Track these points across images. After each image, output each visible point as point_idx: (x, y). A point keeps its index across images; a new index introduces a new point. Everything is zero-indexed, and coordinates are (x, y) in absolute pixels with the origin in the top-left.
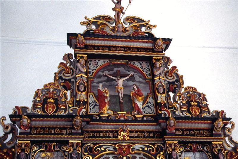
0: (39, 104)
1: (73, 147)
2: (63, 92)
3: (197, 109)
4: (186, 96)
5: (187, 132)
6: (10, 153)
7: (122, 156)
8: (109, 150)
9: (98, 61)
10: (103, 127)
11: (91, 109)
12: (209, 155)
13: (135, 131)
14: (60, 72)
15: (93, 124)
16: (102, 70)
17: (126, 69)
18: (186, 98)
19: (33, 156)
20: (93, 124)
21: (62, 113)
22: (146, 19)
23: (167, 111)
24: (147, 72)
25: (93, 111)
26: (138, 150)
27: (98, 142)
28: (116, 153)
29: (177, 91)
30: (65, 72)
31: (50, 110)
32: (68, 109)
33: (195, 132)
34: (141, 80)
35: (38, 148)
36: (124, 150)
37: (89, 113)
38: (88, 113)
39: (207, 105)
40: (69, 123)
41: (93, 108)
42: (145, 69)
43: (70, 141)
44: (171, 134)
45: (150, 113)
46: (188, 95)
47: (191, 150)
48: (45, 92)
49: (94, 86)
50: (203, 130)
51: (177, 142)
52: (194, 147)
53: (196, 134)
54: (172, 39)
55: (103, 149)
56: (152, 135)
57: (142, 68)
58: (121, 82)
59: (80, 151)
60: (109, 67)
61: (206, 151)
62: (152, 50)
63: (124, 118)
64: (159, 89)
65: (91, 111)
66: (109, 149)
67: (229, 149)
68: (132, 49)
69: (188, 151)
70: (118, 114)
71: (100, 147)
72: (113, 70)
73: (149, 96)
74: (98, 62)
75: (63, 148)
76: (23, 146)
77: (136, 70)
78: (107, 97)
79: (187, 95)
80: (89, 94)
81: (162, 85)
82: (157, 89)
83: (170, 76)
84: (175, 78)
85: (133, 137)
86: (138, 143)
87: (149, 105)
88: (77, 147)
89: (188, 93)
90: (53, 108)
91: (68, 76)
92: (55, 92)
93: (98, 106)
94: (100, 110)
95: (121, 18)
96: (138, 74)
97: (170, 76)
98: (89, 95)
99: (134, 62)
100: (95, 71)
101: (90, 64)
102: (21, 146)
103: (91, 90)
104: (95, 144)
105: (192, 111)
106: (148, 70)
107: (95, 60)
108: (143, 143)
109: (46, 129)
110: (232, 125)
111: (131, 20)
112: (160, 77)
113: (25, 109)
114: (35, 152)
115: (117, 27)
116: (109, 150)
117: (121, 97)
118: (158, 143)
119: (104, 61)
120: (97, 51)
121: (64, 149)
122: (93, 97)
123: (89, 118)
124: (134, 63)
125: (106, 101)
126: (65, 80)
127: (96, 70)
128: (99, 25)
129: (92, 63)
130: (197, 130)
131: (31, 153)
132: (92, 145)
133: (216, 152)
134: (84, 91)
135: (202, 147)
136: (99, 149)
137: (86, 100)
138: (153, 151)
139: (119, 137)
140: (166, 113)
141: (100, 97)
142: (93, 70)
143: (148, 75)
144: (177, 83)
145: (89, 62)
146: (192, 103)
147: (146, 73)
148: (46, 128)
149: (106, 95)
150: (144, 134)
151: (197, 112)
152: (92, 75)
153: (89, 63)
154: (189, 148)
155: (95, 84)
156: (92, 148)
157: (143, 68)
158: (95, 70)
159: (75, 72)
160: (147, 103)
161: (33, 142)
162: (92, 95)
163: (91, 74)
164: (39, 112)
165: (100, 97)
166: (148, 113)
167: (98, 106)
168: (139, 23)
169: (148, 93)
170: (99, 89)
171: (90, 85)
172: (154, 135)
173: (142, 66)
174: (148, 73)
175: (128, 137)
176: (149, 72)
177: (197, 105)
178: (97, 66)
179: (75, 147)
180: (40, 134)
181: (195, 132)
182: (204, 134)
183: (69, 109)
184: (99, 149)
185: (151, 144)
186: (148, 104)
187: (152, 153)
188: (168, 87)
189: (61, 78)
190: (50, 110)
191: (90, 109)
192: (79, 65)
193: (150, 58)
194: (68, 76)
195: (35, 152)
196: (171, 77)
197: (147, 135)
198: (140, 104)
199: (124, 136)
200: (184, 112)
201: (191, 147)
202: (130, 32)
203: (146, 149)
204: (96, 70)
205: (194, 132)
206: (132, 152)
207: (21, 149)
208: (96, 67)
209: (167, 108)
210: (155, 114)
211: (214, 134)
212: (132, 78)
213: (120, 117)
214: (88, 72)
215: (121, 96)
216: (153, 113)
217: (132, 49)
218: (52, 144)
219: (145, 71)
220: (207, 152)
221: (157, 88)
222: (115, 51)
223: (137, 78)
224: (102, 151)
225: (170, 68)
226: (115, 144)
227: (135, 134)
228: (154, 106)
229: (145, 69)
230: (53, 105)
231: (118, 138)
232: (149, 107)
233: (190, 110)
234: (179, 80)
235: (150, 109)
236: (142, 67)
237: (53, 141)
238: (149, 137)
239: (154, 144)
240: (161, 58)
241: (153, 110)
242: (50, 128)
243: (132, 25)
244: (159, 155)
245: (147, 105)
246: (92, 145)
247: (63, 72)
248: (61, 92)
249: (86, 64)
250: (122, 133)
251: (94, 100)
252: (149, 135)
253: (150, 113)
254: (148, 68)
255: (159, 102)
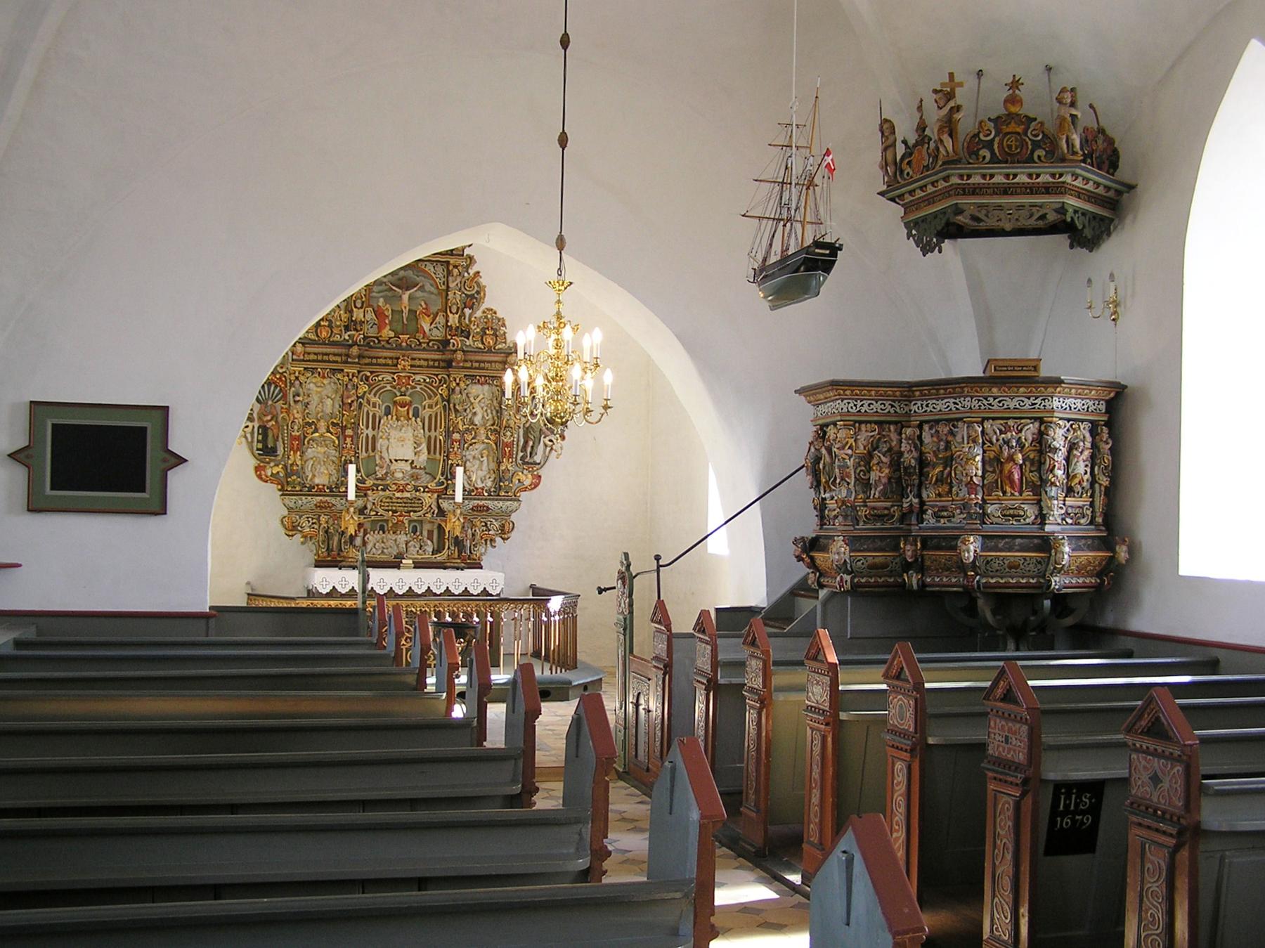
1: (348, 376)
3: (492, 339)
5: (477, 365)
23: (456, 341)
34: (433, 289)
39: (505, 333)
55: (380, 379)
56: (436, 364)
78: (387, 317)
82: (450, 307)
84: (476, 288)
87: (438, 326)
88: (353, 376)
104: (372, 373)
117: (406, 311)
123: (368, 343)
125: (387, 321)
132: (369, 374)
141: (379, 313)
146: (488, 332)
148: (319, 353)
149: (387, 314)
155: (374, 294)
156: (369, 377)
165: (379, 313)
174: (442, 282)
190: (324, 334)
193: (448, 263)
197: (431, 363)
198: (426, 327)
199: (404, 366)
203: (428, 380)
220: (497, 386)
224: (379, 381)
226: (394, 373)
239: (437, 375)
246: (369, 374)
255: (449, 324)
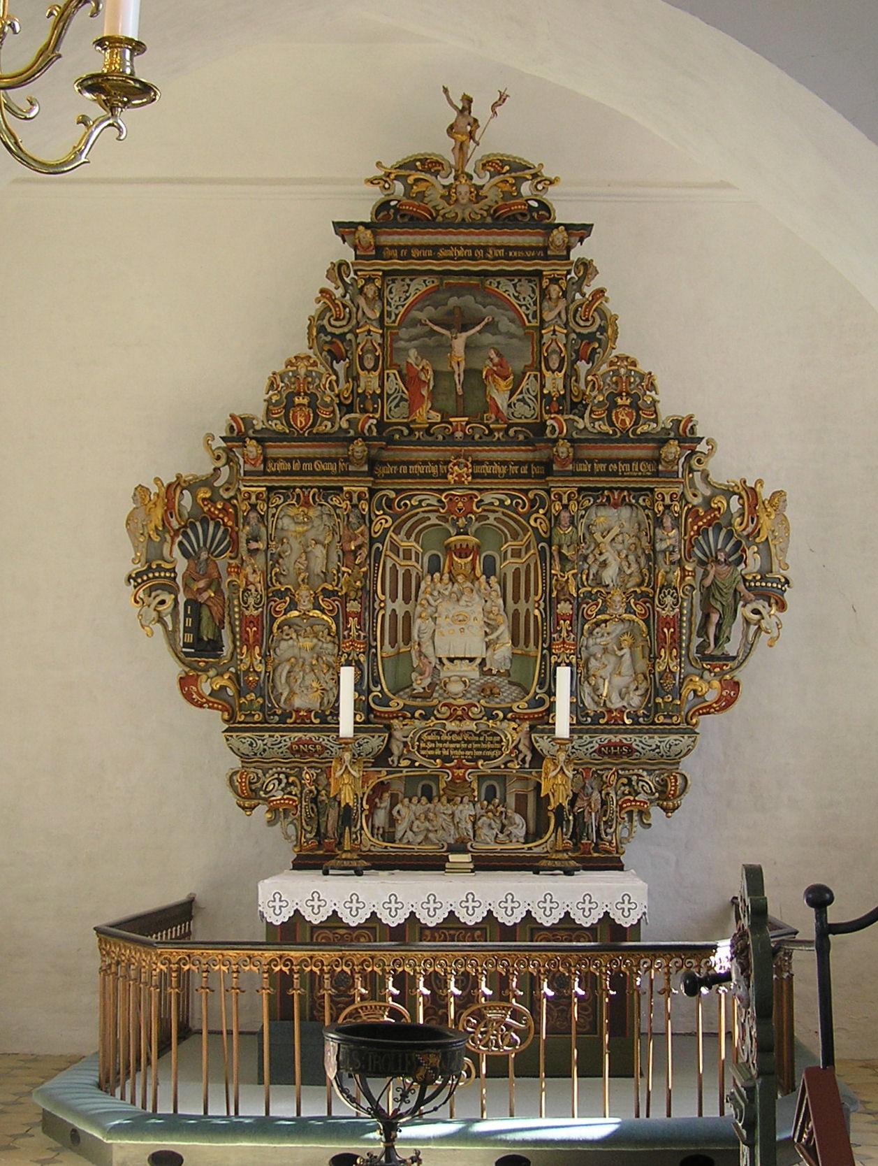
0: (245, 786)
2: (327, 378)
4: (608, 380)
5: (602, 467)
6: (231, 510)
7: (455, 518)
8: (428, 505)
9: (409, 282)
10: (415, 454)
11: (393, 408)
12: (647, 516)
13: (488, 461)
14: (321, 316)
15: (392, 450)
16: (418, 306)
17: (479, 299)
18: (609, 385)
19: (273, 516)
20: (392, 450)
21: (326, 427)
22: (533, 160)
24: (528, 309)
25: (396, 414)
26: (492, 504)
27: (404, 487)
28: (441, 510)
29: (598, 358)
30: (332, 316)
31: (301, 423)
32: (338, 420)
33: (620, 465)
34: (513, 328)
35: (282, 500)
36: (460, 504)
37: (388, 418)
38: (385, 420)
39: (654, 402)
40: (341, 450)
41: (395, 407)
42: (524, 299)
43: (345, 488)
44: (564, 473)
45: (526, 418)
46: (614, 379)
47: (610, 503)
48: (290, 378)
49: (399, 349)
50: (639, 460)
51: (574, 490)
52: (614, 499)
53: (622, 472)
54: (592, 225)
55: (415, 503)
56: (524, 471)
57: (517, 298)
58: (459, 343)
59: (367, 510)
60: (440, 296)
61: (642, 506)
62: (542, 252)
63: (465, 433)
64: (550, 360)
65: (392, 413)
66: (428, 502)
67: (696, 501)
68: (491, 252)
69: (603, 505)
70: (450, 423)
71: (410, 498)
72: (446, 304)
73: (528, 374)
74: (409, 285)
75: (332, 500)
76: (253, 498)
77: (504, 303)
79: (612, 377)
80: (386, 372)
81: (557, 349)
82: (546, 359)
83: (584, 318)
84: (598, 321)
85: (481, 476)
86: (492, 489)
87: (526, 396)
88: (359, 501)
89: (616, 373)
90: (307, 420)
91: (341, 327)
92: (310, 379)
93: (406, 400)
94: (410, 413)
95: (469, 156)
96: (506, 313)
97: (584, 318)
98: (388, 374)
99: (498, 279)
100: (402, 310)
101: (391, 292)
102: (249, 498)
103: (391, 360)
104: (398, 492)
105: (617, 418)
106: (531, 302)
107: (403, 280)
108: (503, 489)
109: (296, 462)
110: (710, 447)
111: (495, 165)
112: (557, 328)
113: (247, 421)
114: (277, 507)
115: (455, 193)
116: (428, 505)
118: (537, 489)
119: (425, 281)
120: (405, 262)
121: (335, 501)
122: (396, 379)
124: (499, 283)
125: (424, 392)
126: (333, 335)
127: (406, 307)
128: (412, 186)
129: (395, 286)
130: (625, 461)
131: (270, 509)
132: (392, 495)
133: (659, 511)
134: (375, 369)
135: (633, 498)
136: (408, 502)
137: (378, 392)
138: (523, 508)
139: (450, 477)
140: (555, 424)
141: (411, 379)
142: (397, 308)
143: (530, 317)
144: (601, 334)
145: (388, 285)
147: (527, 312)
150: (508, 467)
151: (628, 423)
152: (394, 322)
153: (389, 287)
154: (604, 501)
155: (402, 344)
157: (521, 297)
158: (403, 306)
159: (355, 315)
160: (521, 393)
161: (270, 489)
162: (394, 374)
163: (393, 318)
164: (279, 427)
165: (411, 379)
166: (521, 418)
167: (406, 400)
168: (513, 174)
169: (527, 364)
170: (410, 361)
171: (391, 346)
172: (529, 470)
173: (517, 292)
175: (470, 478)
176: (535, 308)
177: (630, 406)
178: (408, 294)
179: (355, 500)
180: (284, 473)
181: (620, 465)
182: (640, 470)
183: (341, 419)
184: (408, 502)
185: (520, 490)
186: (524, 395)
187: (521, 510)
188: (577, 348)
189: (322, 329)
191: (390, 410)
192: (361, 301)
194: (341, 327)
195: (277, 507)
196: (587, 320)
197: (514, 469)
199: (460, 476)
200: (597, 423)
201: (608, 497)
202: (492, 200)
204: (406, 307)
205: (618, 466)
206: (478, 508)
207: (250, 504)
208: (405, 300)
209: (477, 497)
210: (536, 418)
211: (662, 471)
212: (492, 327)
213: (455, 430)
214: (386, 313)
215: (459, 380)
216: (532, 416)
217: (491, 252)
218: (309, 492)
219: (525, 305)
220: (645, 508)
221: (545, 357)
222: (448, 261)
223: (505, 324)
224: (413, 507)
225: (588, 291)
227: (487, 467)
228: (537, 400)
229: (524, 299)
230: (306, 410)
231: (447, 478)
232: (526, 403)
233: (611, 416)
234: (606, 328)
235: (526, 406)
236: (516, 294)
237: (312, 488)
238: (519, 476)
239: (526, 492)
240: (565, 272)
241: (534, 409)
242: (303, 460)
243: (497, 179)
244: (535, 515)
245: (520, 397)
246: (392, 495)
247: (328, 314)
248: (324, 380)
249: (380, 293)
250: (456, 468)
251: (397, 387)
252: (519, 470)
253: (526, 418)
254: (532, 295)
